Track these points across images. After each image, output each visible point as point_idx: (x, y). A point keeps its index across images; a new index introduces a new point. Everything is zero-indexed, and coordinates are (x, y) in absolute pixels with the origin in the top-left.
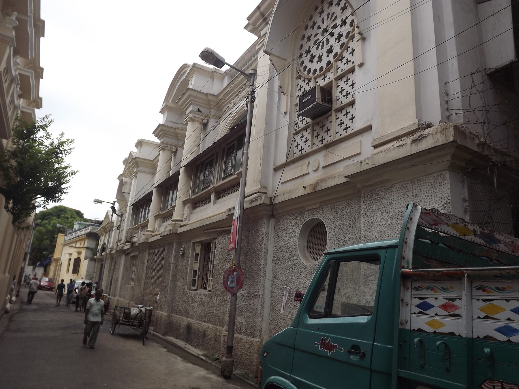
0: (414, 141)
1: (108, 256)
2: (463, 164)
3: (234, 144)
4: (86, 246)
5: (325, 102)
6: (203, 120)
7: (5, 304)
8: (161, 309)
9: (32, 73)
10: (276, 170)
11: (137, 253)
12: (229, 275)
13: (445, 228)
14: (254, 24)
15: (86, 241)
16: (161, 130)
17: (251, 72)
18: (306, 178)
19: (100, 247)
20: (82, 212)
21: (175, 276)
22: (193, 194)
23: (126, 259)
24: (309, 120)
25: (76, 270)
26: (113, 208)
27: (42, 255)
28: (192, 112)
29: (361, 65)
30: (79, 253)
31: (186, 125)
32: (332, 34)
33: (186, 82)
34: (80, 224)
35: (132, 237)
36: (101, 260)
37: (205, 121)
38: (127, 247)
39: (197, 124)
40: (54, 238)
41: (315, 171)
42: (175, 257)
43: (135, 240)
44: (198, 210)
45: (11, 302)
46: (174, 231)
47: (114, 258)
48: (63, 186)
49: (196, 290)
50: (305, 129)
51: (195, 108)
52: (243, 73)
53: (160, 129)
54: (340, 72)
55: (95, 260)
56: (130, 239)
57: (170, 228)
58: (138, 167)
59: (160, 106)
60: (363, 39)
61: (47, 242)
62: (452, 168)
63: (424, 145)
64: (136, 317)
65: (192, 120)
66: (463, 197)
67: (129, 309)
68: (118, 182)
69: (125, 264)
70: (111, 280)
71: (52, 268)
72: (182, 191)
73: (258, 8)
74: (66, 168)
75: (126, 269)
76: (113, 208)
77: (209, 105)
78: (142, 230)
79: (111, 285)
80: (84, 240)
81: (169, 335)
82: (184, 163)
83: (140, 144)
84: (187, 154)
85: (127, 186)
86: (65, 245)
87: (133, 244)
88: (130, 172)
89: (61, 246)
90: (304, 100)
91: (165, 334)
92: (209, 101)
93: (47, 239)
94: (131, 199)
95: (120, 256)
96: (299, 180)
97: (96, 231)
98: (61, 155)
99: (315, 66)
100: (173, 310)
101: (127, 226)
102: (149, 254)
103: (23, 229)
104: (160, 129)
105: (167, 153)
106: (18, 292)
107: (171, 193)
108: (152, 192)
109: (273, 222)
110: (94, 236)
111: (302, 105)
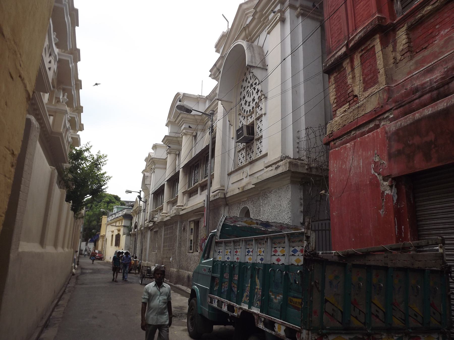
0: (276, 168)
1: (139, 232)
2: (300, 180)
3: (352, 35)
4: (123, 225)
5: (250, 135)
6: (193, 133)
7: (72, 270)
8: (173, 267)
9: (76, 115)
10: (229, 174)
11: (158, 229)
12: (203, 242)
14: (214, 74)
15: (123, 221)
16: (167, 140)
17: (211, 112)
18: (243, 181)
19: (133, 225)
20: (119, 196)
21: (180, 244)
22: (189, 187)
23: (151, 234)
24: (245, 144)
25: (117, 244)
26: (139, 197)
27: (92, 233)
28: (184, 128)
29: (265, 114)
30: (119, 230)
31: (182, 137)
32: (254, 89)
34: (118, 208)
35: (153, 218)
36: (135, 235)
37: (194, 134)
38: (151, 225)
41: (246, 177)
42: (179, 231)
43: (155, 219)
44: (192, 198)
45: (75, 268)
46: (177, 214)
47: (143, 233)
48: (103, 188)
49: (192, 253)
50: (243, 149)
51: (187, 126)
52: (205, 114)
53: (166, 139)
54: (258, 116)
56: (152, 219)
57: (174, 212)
58: (155, 165)
59: (165, 122)
60: (266, 98)
61: (95, 223)
62: (293, 182)
63: (280, 171)
65: (185, 134)
66: (300, 197)
67: (150, 267)
68: (142, 175)
69: (151, 237)
70: (142, 249)
71: (100, 243)
72: (181, 186)
73: (215, 65)
74: (103, 174)
75: (151, 241)
76: (139, 197)
77: (197, 122)
78: (160, 212)
79: (142, 253)
80: (121, 220)
81: (178, 284)
82: (182, 166)
83: (155, 147)
84: (184, 159)
85: (149, 179)
86: (108, 225)
87: (154, 222)
88: (150, 168)
89: (105, 226)
90: (239, 132)
91: (176, 283)
92: (196, 120)
93: (94, 220)
94: (153, 188)
95: (147, 232)
96: (239, 182)
97: (130, 211)
98: (99, 166)
99: (247, 108)
100: (181, 267)
101: (150, 209)
102: (165, 229)
103: (79, 218)
104: (166, 139)
105: (173, 156)
106: (78, 262)
107: (194, 171)
109: (227, 208)
110: (128, 217)
111: (238, 136)
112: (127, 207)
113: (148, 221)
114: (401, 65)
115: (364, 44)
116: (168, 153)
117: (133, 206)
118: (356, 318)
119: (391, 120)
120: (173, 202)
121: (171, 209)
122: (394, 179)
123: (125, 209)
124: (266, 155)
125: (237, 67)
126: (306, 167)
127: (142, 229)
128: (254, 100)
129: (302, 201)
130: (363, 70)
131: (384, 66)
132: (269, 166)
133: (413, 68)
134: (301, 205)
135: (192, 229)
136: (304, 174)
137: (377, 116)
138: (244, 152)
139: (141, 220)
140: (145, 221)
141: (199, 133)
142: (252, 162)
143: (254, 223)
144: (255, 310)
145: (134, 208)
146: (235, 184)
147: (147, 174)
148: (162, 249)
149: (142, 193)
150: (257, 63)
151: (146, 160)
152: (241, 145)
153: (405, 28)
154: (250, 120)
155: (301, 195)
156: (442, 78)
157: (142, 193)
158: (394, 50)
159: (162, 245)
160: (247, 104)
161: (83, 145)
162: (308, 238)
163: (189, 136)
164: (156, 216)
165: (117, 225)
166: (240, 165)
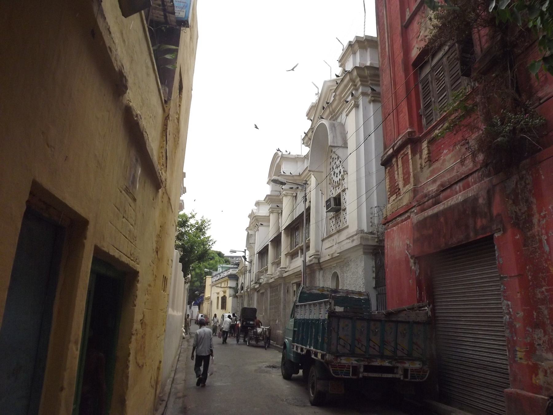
1: (246, 293)
5: (337, 206)
8: (279, 330)
10: (323, 240)
13: (314, 291)
15: (229, 282)
16: (269, 199)
20: (223, 252)
21: (285, 306)
22: (291, 249)
23: (258, 296)
25: (224, 307)
30: (225, 292)
31: (283, 198)
33: (279, 166)
35: (259, 279)
37: (295, 195)
38: (257, 286)
39: (289, 197)
40: (202, 279)
43: (261, 281)
44: (294, 260)
55: (237, 297)
57: (278, 274)
59: (267, 180)
60: (347, 174)
61: (198, 284)
63: (355, 243)
64: (261, 334)
65: (286, 196)
69: (258, 299)
82: (284, 227)
83: (258, 204)
84: (286, 221)
85: (253, 238)
86: (213, 286)
87: (260, 283)
93: (197, 281)
94: (258, 248)
95: (253, 293)
99: (336, 179)
108: (268, 245)
109: (322, 272)
111: (328, 206)
112: (232, 266)
113: (254, 282)
114: (425, 170)
115: (403, 149)
116: (272, 212)
117: (238, 264)
118: (360, 349)
119: (417, 214)
120: (277, 263)
121: (275, 270)
122: (416, 258)
123: (230, 268)
124: (347, 227)
125: (323, 142)
126: (376, 240)
127: (249, 290)
128: (340, 172)
129: (374, 269)
130: (403, 170)
131: (413, 171)
132: (350, 237)
133: (429, 175)
134: (373, 272)
135: (294, 291)
136: (375, 246)
137: (408, 209)
138: (334, 220)
139: (247, 280)
140: (251, 282)
141: (298, 193)
142: (339, 231)
143: (325, 291)
144: (312, 348)
145: (240, 268)
146: (327, 250)
147: (250, 232)
148: (268, 311)
149: (247, 252)
150: (340, 143)
151: (250, 216)
152: (332, 214)
153: (426, 142)
154: (338, 191)
155: (373, 263)
156: (437, 190)
157: (247, 252)
158: (421, 158)
159: (269, 307)
160: (336, 175)
161: (187, 211)
162: (330, 303)
163: (289, 197)
164: (262, 277)
165: (222, 286)
166: (332, 233)
